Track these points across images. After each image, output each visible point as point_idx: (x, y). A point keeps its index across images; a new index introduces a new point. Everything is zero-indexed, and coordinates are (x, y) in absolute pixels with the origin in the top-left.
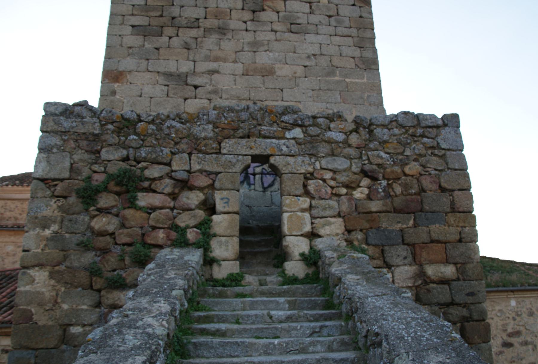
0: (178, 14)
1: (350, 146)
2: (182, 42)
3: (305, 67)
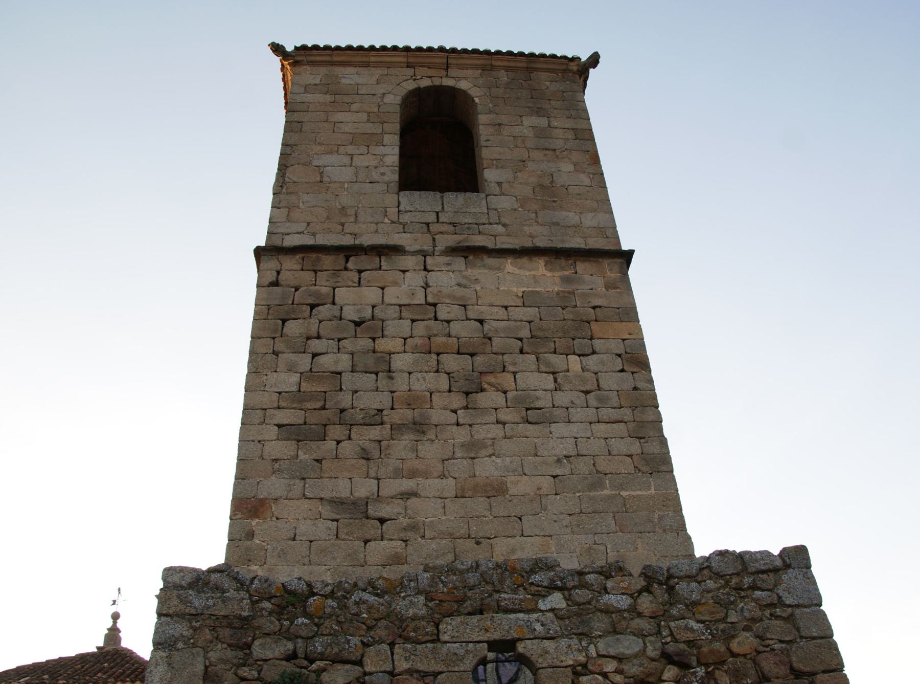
0: (350, 403)
1: (640, 615)
2: (358, 449)
3: (554, 477)
